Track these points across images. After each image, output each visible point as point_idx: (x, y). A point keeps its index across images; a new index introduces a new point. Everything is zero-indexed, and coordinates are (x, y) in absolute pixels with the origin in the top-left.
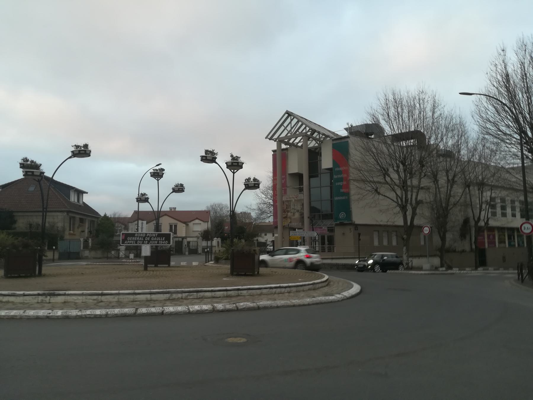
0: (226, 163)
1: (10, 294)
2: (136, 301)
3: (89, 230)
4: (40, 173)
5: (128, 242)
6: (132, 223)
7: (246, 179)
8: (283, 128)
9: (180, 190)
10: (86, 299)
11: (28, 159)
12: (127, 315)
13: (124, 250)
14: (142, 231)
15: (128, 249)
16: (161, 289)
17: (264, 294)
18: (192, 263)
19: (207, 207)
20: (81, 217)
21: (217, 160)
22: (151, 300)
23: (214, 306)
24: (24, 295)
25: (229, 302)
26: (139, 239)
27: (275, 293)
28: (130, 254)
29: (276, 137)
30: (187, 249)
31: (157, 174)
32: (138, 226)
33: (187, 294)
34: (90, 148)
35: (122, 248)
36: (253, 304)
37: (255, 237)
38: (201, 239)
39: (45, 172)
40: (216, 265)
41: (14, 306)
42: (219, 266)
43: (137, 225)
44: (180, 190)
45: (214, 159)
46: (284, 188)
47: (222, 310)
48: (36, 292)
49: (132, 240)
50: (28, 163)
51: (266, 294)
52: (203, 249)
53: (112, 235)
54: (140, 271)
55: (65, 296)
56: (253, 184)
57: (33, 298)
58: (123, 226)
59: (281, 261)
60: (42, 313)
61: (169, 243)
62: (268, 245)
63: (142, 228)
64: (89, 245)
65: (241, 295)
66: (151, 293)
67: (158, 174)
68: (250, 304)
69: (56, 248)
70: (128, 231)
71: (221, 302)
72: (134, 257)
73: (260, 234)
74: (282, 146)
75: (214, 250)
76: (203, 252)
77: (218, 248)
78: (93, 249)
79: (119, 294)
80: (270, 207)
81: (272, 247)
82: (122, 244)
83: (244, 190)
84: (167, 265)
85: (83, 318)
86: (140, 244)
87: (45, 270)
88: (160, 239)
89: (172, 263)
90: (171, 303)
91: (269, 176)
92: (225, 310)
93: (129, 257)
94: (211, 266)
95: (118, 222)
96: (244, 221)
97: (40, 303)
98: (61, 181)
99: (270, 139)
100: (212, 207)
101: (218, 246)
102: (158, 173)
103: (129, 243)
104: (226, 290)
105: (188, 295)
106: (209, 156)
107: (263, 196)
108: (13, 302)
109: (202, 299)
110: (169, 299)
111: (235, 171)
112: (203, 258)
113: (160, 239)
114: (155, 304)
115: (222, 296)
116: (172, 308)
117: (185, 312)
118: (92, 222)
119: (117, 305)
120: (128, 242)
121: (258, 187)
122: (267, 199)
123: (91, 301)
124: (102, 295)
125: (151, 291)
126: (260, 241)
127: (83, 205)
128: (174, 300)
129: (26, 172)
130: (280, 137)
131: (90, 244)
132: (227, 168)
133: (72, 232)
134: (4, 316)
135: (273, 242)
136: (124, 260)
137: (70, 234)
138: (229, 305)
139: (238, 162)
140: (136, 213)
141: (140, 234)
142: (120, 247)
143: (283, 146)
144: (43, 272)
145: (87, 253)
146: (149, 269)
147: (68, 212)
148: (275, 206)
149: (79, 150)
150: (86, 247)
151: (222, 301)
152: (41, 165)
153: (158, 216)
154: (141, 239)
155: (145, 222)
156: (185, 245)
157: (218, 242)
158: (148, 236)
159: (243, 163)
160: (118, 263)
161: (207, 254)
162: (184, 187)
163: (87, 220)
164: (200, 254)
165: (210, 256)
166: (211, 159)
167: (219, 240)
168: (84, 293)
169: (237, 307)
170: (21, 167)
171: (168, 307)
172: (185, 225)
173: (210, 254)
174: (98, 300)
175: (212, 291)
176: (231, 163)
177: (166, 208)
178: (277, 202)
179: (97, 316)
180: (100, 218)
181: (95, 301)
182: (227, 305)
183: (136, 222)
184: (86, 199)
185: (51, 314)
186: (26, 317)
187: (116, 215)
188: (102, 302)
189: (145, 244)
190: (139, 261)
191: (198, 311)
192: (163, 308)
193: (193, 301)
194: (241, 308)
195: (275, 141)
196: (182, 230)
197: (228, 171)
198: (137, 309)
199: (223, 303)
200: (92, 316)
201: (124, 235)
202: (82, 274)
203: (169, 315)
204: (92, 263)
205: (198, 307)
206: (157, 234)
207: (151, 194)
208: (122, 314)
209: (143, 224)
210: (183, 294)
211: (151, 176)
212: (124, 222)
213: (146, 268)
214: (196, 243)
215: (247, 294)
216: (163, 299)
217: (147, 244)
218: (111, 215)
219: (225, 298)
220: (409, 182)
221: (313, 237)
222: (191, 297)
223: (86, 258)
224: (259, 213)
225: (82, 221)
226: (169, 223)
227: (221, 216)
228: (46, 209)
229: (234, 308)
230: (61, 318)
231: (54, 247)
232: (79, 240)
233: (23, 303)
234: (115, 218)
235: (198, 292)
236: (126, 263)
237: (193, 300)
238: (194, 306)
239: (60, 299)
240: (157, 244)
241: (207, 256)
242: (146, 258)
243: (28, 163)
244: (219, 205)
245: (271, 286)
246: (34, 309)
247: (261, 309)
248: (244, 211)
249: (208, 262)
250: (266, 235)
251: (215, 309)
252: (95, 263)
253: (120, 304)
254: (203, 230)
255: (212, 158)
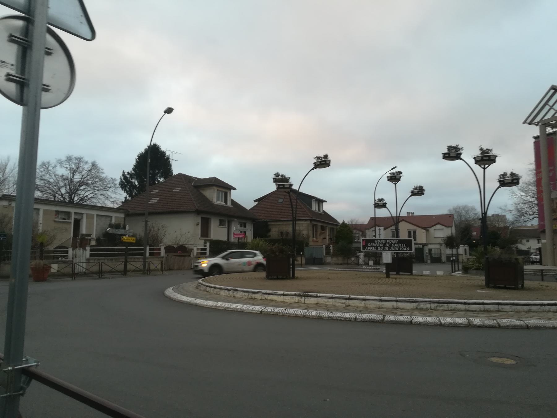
0: (474, 158)
1: (273, 293)
2: (382, 308)
3: (330, 237)
4: (289, 185)
5: (369, 248)
6: (369, 230)
7: (501, 175)
8: (547, 108)
9: (419, 192)
10: (335, 302)
11: (279, 174)
12: (375, 321)
13: (363, 256)
14: (380, 238)
15: (367, 255)
16: (407, 297)
17: (533, 312)
18: (436, 273)
19: (450, 210)
20: (322, 225)
21: (462, 156)
22: (397, 308)
23: (469, 320)
24: (284, 295)
25: (487, 317)
26: (380, 245)
27: (549, 311)
28: (370, 261)
29: (538, 119)
30: (429, 257)
31: (394, 178)
32: (375, 233)
33: (436, 304)
34: (330, 158)
35: (361, 255)
36: (519, 322)
37: (513, 244)
38: (445, 246)
39: (293, 184)
40: (464, 275)
41: (277, 304)
42: (469, 276)
43: (374, 232)
45: (459, 156)
46: (552, 183)
47: (479, 325)
48: (293, 293)
49: (372, 247)
50: (280, 177)
51: (537, 312)
52: (448, 258)
53: (351, 242)
54: (383, 278)
55: (317, 298)
56: (511, 180)
57: (291, 298)
58: (361, 233)
59: (240, 265)
60: (300, 312)
61: (411, 250)
62: (532, 254)
63: (380, 235)
64: (330, 251)
65: (502, 310)
66: (397, 301)
67: (395, 178)
68: (516, 322)
69: (303, 254)
70: (365, 237)
71: (478, 316)
72: (374, 264)
73: (519, 241)
74: (547, 130)
75: (460, 259)
76: (447, 261)
77: (465, 256)
78: (334, 255)
79: (365, 300)
80: (532, 207)
81: (538, 257)
82: (363, 250)
83: (499, 188)
84: (410, 274)
85: (335, 320)
86: (380, 250)
87: (299, 272)
88: (401, 245)
89: (414, 272)
90: (419, 313)
91: (530, 170)
92: (484, 325)
93: (368, 264)
94: (460, 276)
95: (355, 229)
96: (497, 225)
97: (297, 302)
98: (307, 193)
99: (530, 123)
100: (456, 210)
101: (466, 254)
102: (395, 176)
103: (369, 250)
104: (483, 304)
105: (437, 305)
106: (453, 153)
107: (523, 194)
108: (276, 300)
109: (454, 312)
110: (416, 309)
111: (486, 166)
112: (449, 267)
113: (401, 245)
114: (401, 312)
115: (478, 310)
116: (422, 318)
117: (436, 324)
118: (332, 230)
119: (365, 310)
120: (369, 248)
121: (518, 183)
122: (528, 198)
123: (340, 304)
124: (350, 299)
125: (397, 299)
126: (521, 249)
127: (323, 213)
128: (422, 309)
129: (279, 185)
130: (543, 119)
131: (332, 251)
132: (476, 163)
133: (315, 239)
134: (270, 312)
135: (539, 250)
136: (364, 267)
137: (313, 241)
138: (489, 320)
139: (490, 156)
140: (373, 219)
141: (378, 240)
142: (359, 254)
143: (549, 130)
144: (296, 275)
145: (329, 259)
146: (391, 276)
147: (311, 220)
148: (540, 205)
149: (320, 161)
150: (328, 253)
151: (479, 316)
152: (289, 178)
153: (397, 221)
154: (381, 245)
155: (382, 228)
156: (426, 253)
157: (465, 250)
158: (389, 243)
159: (496, 156)
160: (359, 270)
161: (453, 263)
162: (424, 189)
163: (327, 228)
164: (444, 263)
165: (456, 265)
166: (455, 155)
167: (467, 247)
168: (333, 297)
169: (498, 323)
170: (274, 182)
171: (417, 317)
172: (425, 231)
173: (456, 263)
174: (346, 304)
175: (465, 303)
176: (480, 157)
177: (404, 214)
178: (543, 201)
179: (346, 319)
180: (339, 225)
181: (344, 305)
182: (486, 320)
183: (373, 229)
184: (326, 208)
185: (307, 314)
186: (287, 315)
187: (353, 222)
188: (349, 306)
189: (385, 250)
190: (379, 268)
191: (450, 323)
192: (411, 317)
193: (444, 313)
194: (504, 325)
195: (537, 125)
196: (421, 237)
197: (478, 169)
198: (384, 316)
199: (479, 317)
200: (343, 319)
201: (365, 241)
202: (328, 278)
203: (418, 325)
204: (335, 269)
205: (451, 319)
206: (397, 240)
207: (389, 199)
208: (370, 319)
209: (381, 230)
210: (431, 304)
211: (389, 180)
212: (362, 228)
213: (388, 276)
214: (439, 250)
215: (511, 310)
216: (411, 308)
217: (388, 250)
218: (348, 223)
219: (482, 313)
221: (540, 238)
222: (441, 308)
223: (329, 264)
224: (519, 214)
225: (323, 228)
226: (408, 229)
227: (466, 220)
228: (295, 217)
229: (494, 325)
230: (315, 318)
231: (301, 253)
232: (322, 246)
233: (284, 302)
234: (352, 225)
235: (448, 303)
236: (366, 270)
237: (443, 312)
238: (445, 318)
239: (313, 300)
241: (453, 265)
242: (387, 265)
243: (280, 177)
244: (464, 207)
245: (542, 303)
246: (293, 308)
247: (530, 329)
248: (497, 213)
249: (455, 271)
250: (528, 241)
251: (472, 324)
252: (337, 269)
253: (367, 310)
254: (446, 237)
255: (456, 154)
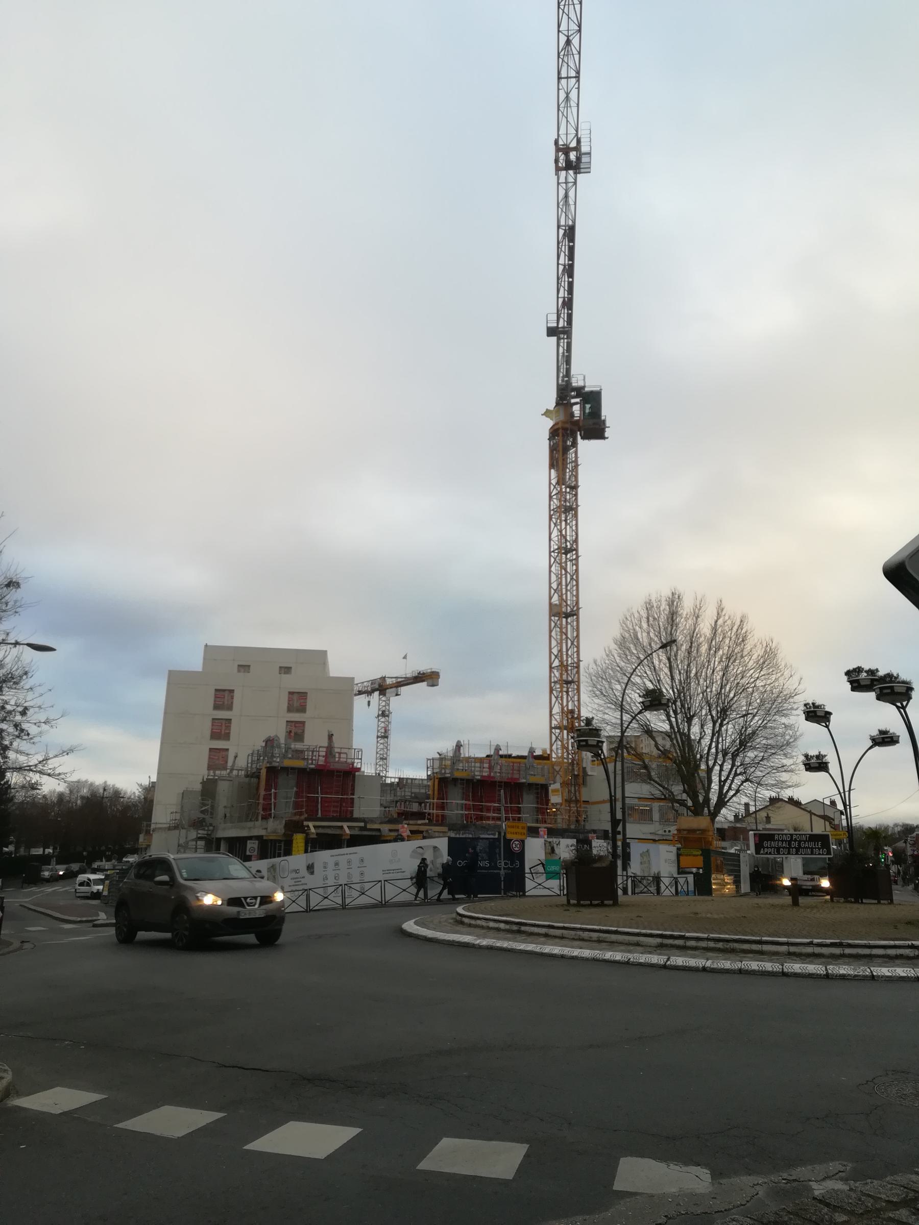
14: (812, 831)
44: (886, 740)
61: (829, 853)
83: (871, 748)
88: (815, 845)
103: (767, 853)
113: (815, 845)
154: (784, 845)
158: (796, 840)
189: (792, 854)
206: (808, 836)
220: (556, 720)
240: (811, 855)
